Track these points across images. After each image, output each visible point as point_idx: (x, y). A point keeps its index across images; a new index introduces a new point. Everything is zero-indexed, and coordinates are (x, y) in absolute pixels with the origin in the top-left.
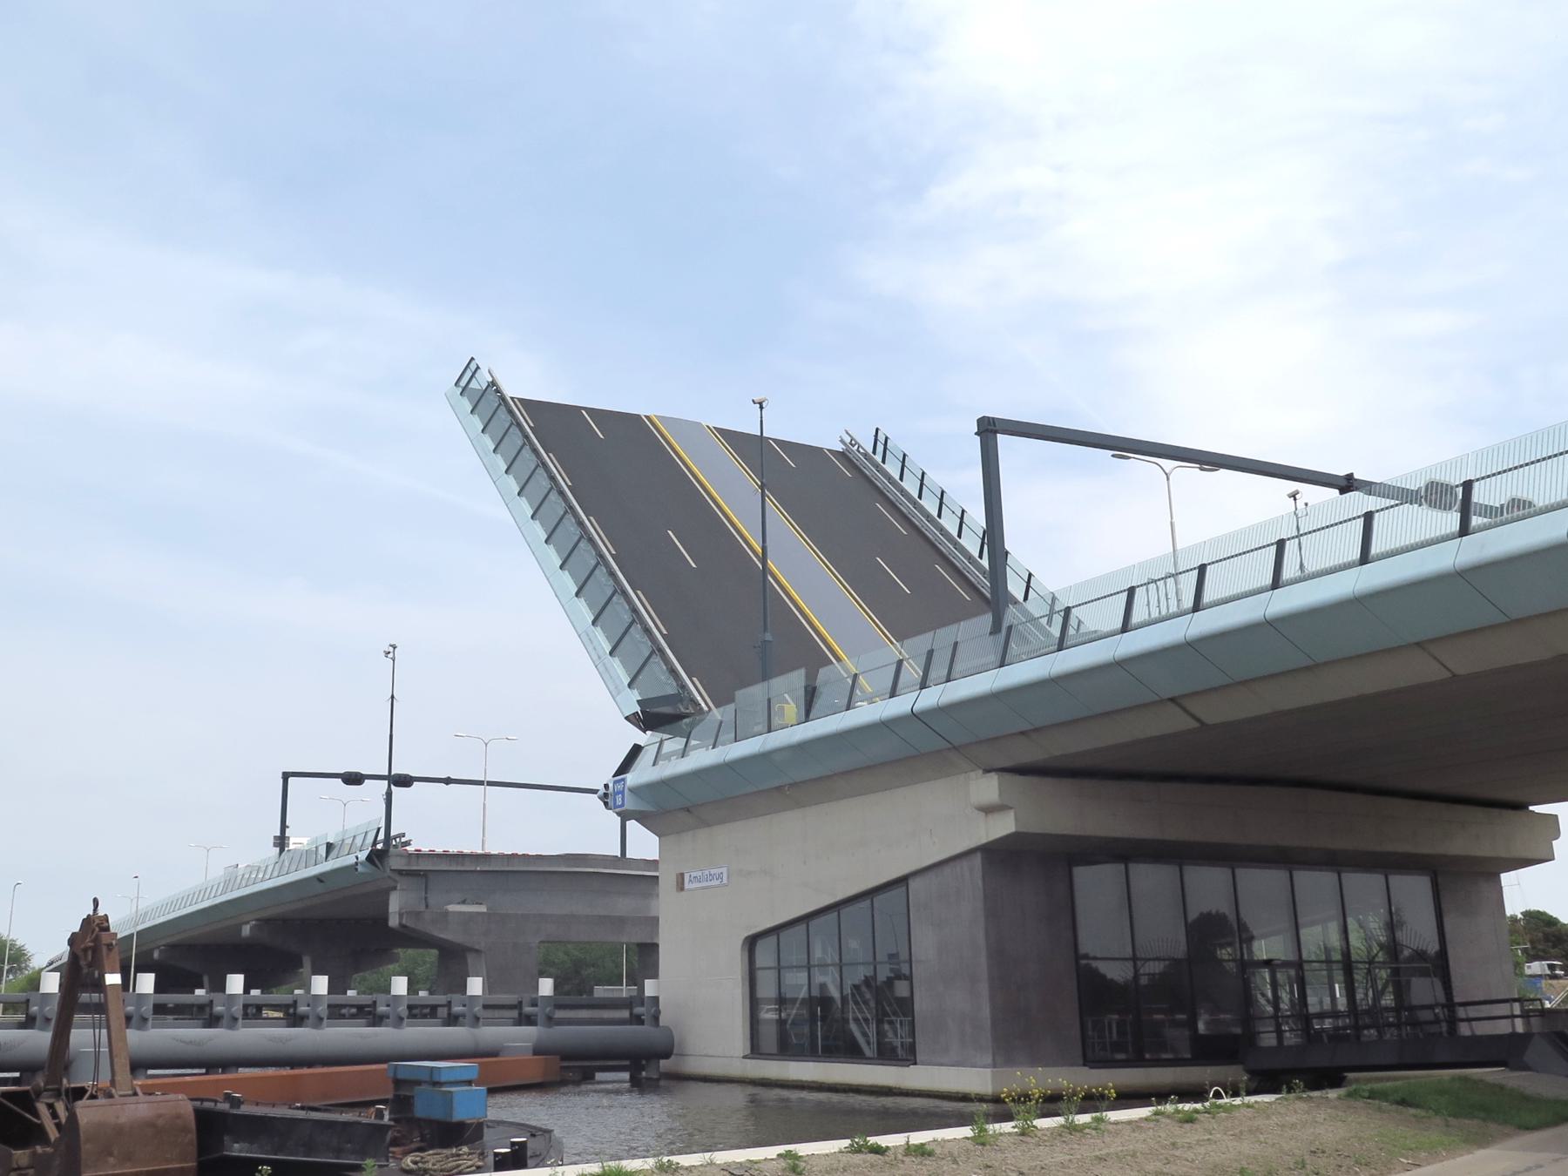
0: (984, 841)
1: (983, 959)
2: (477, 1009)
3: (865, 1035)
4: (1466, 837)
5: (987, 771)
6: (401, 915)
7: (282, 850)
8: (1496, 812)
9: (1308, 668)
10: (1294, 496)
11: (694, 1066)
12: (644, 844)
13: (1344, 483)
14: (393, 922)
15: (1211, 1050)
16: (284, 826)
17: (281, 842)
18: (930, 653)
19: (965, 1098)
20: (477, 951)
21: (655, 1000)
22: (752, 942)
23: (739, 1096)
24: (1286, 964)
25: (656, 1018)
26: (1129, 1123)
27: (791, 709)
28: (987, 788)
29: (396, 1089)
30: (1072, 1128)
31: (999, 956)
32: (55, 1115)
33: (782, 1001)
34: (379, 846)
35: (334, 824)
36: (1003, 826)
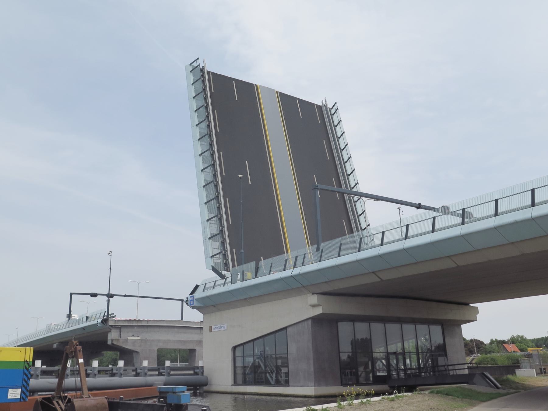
0: (312, 316)
1: (312, 352)
2: (122, 371)
3: (271, 377)
4: (452, 314)
5: (313, 294)
6: (112, 340)
7: (69, 319)
8: (460, 306)
9: (415, 263)
10: (399, 209)
11: (214, 388)
12: (194, 316)
13: (418, 206)
14: (109, 343)
15: (378, 380)
16: (70, 311)
17: (69, 316)
18: (297, 257)
19: (305, 397)
20: (137, 352)
21: (202, 367)
22: (235, 348)
23: (229, 397)
24: (400, 353)
25: (202, 373)
26: (376, 401)
27: (249, 275)
28: (314, 299)
29: (160, 394)
30: (362, 403)
31: (317, 351)
32: (59, 405)
33: (244, 367)
34: (105, 318)
35: (88, 312)
36: (319, 311)
